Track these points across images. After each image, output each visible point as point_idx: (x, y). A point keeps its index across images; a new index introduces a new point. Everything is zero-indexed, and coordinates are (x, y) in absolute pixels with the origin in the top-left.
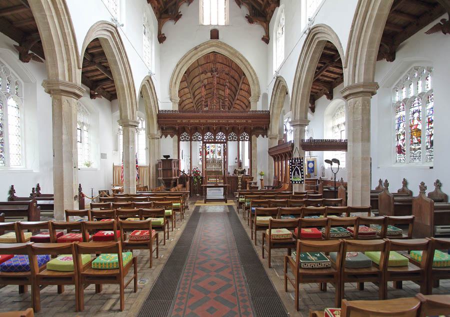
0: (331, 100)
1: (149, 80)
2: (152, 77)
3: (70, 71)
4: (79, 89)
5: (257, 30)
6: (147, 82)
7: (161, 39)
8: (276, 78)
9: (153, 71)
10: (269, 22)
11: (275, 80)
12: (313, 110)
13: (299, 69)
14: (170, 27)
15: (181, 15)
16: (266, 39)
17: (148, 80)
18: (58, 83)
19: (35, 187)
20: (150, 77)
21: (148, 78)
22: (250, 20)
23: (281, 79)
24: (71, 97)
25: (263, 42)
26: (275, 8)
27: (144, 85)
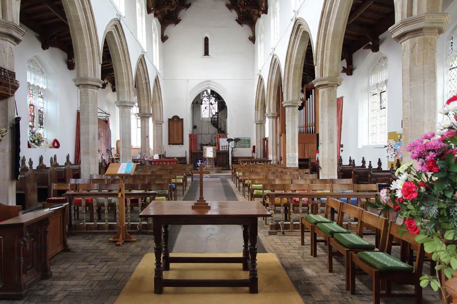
0: (348, 75)
1: (117, 25)
2: (122, 22)
3: (93, 67)
4: (19, 31)
5: (245, 30)
6: (114, 27)
7: (164, 39)
8: (294, 20)
9: (123, 14)
10: (255, 24)
11: (293, 23)
12: (349, 71)
13: (324, 20)
14: (171, 30)
15: (180, 20)
16: (253, 39)
17: (116, 26)
18: (86, 79)
19: (53, 157)
20: (119, 21)
21: (116, 23)
22: (240, 21)
23: (302, 22)
24: (7, 40)
25: (251, 42)
26: (257, 19)
27: (110, 33)
